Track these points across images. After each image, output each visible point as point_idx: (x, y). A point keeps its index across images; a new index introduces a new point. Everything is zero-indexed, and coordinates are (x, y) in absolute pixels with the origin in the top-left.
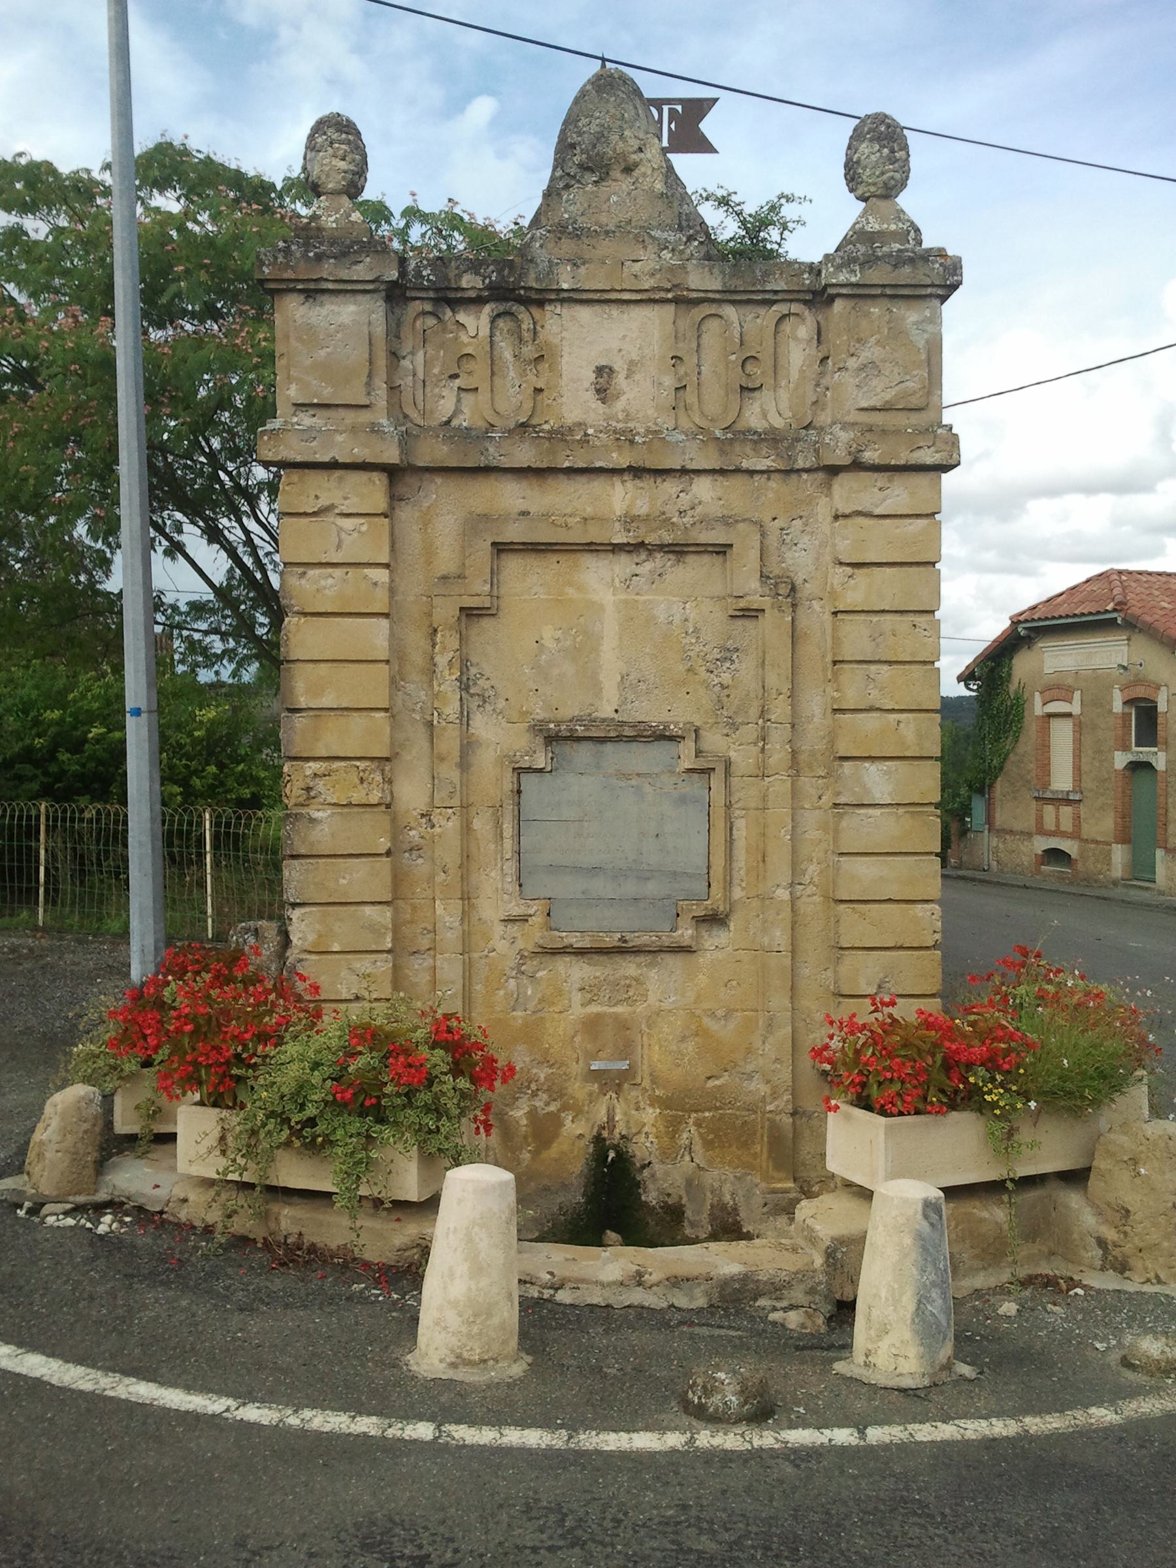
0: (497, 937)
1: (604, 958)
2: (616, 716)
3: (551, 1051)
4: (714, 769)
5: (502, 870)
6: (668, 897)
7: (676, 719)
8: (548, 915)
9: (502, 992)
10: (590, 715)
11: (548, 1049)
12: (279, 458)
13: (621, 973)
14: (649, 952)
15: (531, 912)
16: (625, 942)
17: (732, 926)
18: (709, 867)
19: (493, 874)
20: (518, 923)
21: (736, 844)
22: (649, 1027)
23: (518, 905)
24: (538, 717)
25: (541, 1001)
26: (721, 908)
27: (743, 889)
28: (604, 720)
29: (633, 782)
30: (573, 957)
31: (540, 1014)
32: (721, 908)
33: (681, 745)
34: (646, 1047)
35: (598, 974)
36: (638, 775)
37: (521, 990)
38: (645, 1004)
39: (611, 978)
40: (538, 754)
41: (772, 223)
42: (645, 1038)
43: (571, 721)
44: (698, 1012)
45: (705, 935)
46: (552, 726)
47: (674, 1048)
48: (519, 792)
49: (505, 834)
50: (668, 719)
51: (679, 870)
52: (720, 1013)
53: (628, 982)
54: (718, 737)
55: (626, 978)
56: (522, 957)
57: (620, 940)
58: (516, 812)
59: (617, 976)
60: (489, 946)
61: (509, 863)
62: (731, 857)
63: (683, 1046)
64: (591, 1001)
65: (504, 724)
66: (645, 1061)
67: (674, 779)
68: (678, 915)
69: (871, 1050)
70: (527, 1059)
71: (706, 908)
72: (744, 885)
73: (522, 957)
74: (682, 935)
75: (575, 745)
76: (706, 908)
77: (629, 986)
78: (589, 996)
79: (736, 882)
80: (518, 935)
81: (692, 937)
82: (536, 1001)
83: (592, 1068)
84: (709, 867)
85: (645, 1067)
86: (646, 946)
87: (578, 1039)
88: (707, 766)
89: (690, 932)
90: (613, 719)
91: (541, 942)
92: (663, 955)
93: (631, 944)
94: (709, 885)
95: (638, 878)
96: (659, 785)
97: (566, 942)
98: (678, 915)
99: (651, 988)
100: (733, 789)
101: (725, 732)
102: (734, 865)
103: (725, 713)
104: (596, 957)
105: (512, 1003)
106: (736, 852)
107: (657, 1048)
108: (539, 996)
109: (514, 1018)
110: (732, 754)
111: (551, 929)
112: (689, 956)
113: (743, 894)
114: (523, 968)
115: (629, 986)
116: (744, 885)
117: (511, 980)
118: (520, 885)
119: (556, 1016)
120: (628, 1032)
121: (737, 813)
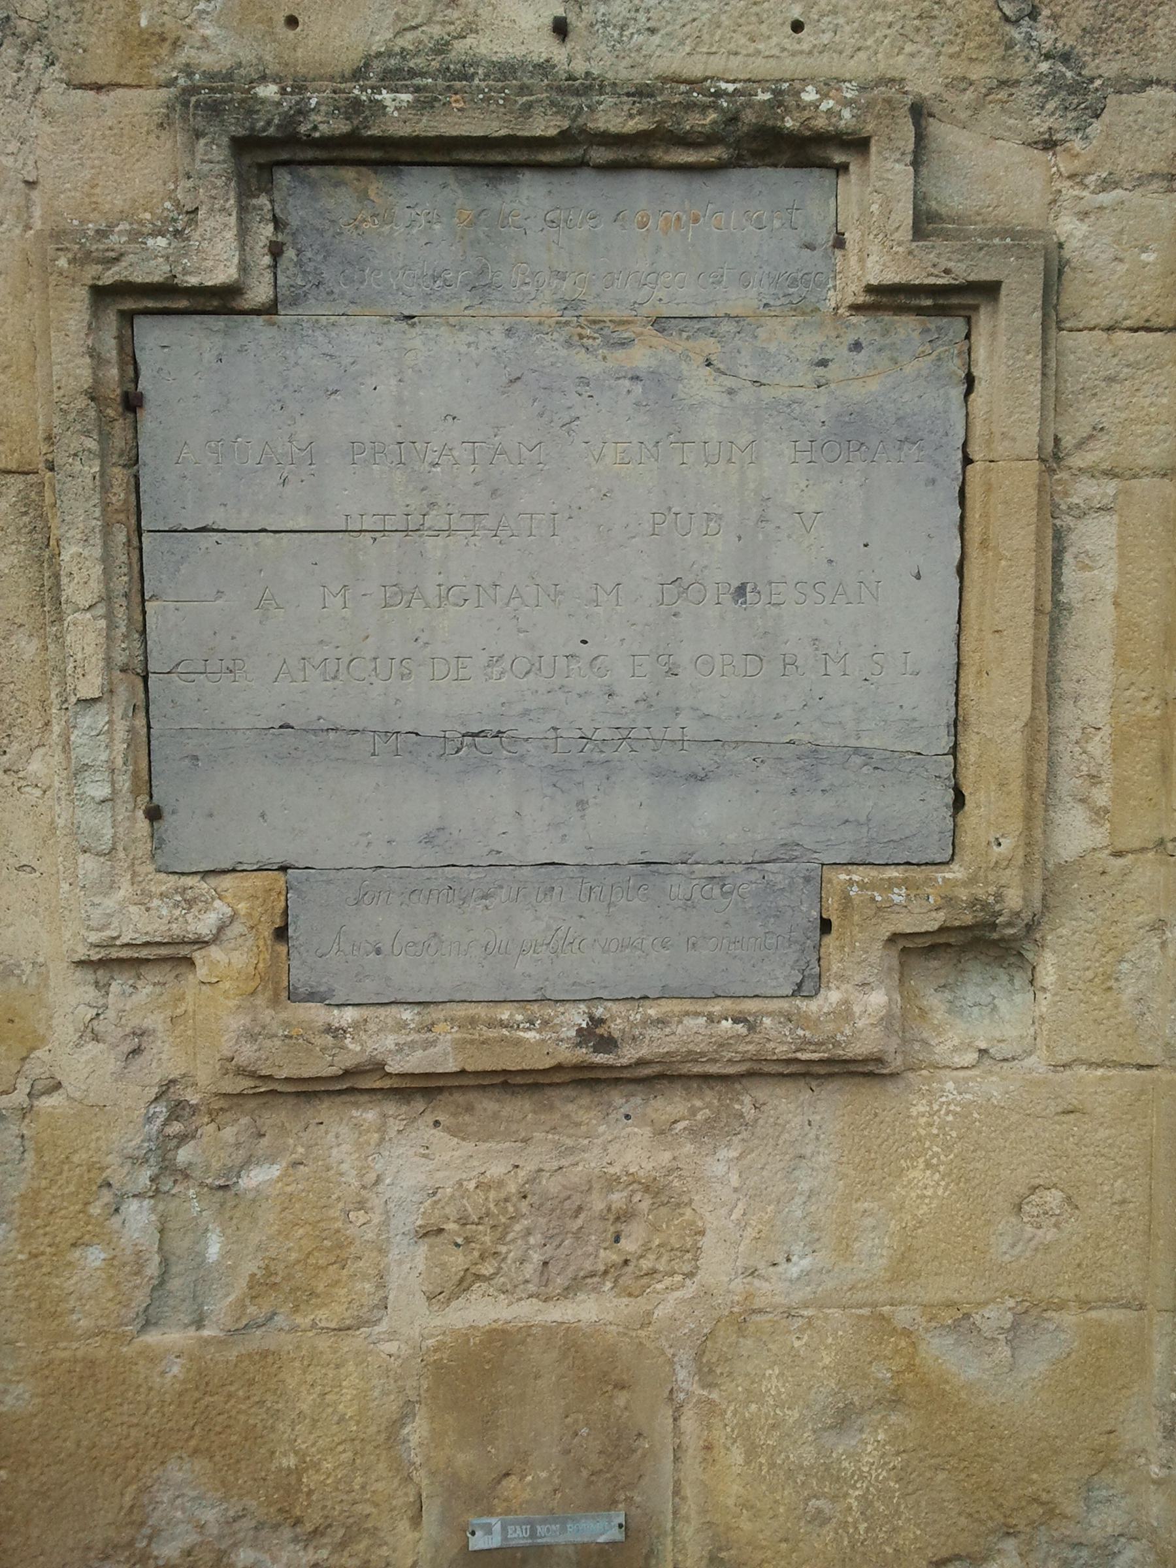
0: (64, 1030)
1: (517, 1108)
2: (558, 53)
3: (310, 1480)
4: (990, 290)
5: (66, 746)
6: (788, 852)
7: (824, 65)
8: (281, 934)
9: (95, 1257)
10: (441, 48)
11: (299, 1472)
12: (112, 94)
13: (591, 1162)
14: (706, 1077)
15: (204, 924)
16: (608, 1043)
17: (1048, 970)
18: (956, 725)
19: (35, 766)
20: (153, 974)
21: (1073, 626)
22: (706, 1374)
23: (143, 899)
24: (207, 60)
25: (261, 1286)
26: (1013, 899)
27: (1099, 814)
28: (505, 70)
29: (640, 358)
30: (391, 1108)
31: (257, 1340)
32: (1013, 899)
33: (850, 187)
34: (691, 1458)
35: (497, 1170)
36: (659, 323)
37: (180, 1244)
38: (691, 1288)
39: (552, 1185)
40: (208, 222)
41: (306, 1470)
42: (689, 1423)
43: (358, 74)
44: (903, 1316)
45: (935, 1002)
46: (269, 91)
47: (808, 1455)
48: (132, 403)
49: (70, 590)
50: (791, 66)
51: (831, 737)
52: (994, 1317)
53: (618, 1198)
54: (1010, 152)
55: (611, 1183)
56: (178, 1110)
57: (584, 1036)
58: (119, 495)
59: (576, 1175)
60: (34, 1069)
61: (89, 720)
62: (1053, 679)
63: (841, 1446)
64: (464, 1283)
65: (54, 94)
66: (690, 1508)
67: (811, 342)
68: (826, 926)
69: (150, 242)
70: (210, 1515)
71: (949, 901)
72: (1101, 796)
73: (178, 1110)
74: (844, 1013)
75: (377, 186)
76: (949, 901)
77: (624, 1216)
78: (458, 1261)
79: (1067, 784)
80: (155, 1021)
81: (887, 1021)
82: (241, 1285)
83: (479, 1542)
84: (956, 725)
85: (688, 1532)
86: (693, 1057)
87: (416, 1431)
88: (964, 271)
89: (877, 999)
90: (544, 68)
91: (247, 1053)
92: (762, 1091)
93: (628, 1054)
94: (959, 801)
95: (659, 774)
96: (749, 371)
97: (355, 1050)
98: (826, 926)
99: (711, 1221)
100: (1070, 386)
101: (1040, 124)
102: (1067, 713)
103: (1045, 37)
104: (487, 1104)
105: (141, 1298)
106: (1072, 661)
107: (737, 1456)
108: (251, 1266)
109: (153, 1357)
110: (1068, 227)
111: (293, 996)
112: (867, 1097)
113: (1099, 836)
114: (184, 1155)
115: (624, 1216)
116: (1101, 796)
117: (132, 1206)
118: (154, 814)
119: (323, 1343)
120: (622, 1399)
121: (1087, 490)
